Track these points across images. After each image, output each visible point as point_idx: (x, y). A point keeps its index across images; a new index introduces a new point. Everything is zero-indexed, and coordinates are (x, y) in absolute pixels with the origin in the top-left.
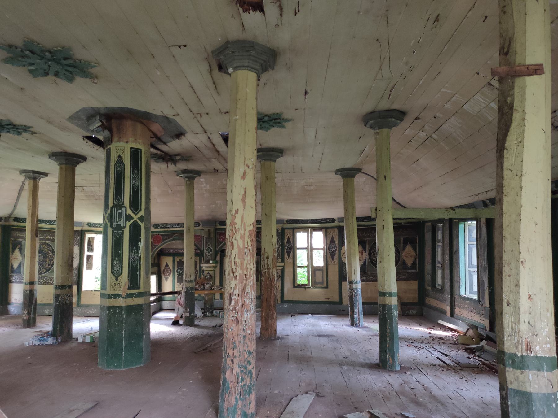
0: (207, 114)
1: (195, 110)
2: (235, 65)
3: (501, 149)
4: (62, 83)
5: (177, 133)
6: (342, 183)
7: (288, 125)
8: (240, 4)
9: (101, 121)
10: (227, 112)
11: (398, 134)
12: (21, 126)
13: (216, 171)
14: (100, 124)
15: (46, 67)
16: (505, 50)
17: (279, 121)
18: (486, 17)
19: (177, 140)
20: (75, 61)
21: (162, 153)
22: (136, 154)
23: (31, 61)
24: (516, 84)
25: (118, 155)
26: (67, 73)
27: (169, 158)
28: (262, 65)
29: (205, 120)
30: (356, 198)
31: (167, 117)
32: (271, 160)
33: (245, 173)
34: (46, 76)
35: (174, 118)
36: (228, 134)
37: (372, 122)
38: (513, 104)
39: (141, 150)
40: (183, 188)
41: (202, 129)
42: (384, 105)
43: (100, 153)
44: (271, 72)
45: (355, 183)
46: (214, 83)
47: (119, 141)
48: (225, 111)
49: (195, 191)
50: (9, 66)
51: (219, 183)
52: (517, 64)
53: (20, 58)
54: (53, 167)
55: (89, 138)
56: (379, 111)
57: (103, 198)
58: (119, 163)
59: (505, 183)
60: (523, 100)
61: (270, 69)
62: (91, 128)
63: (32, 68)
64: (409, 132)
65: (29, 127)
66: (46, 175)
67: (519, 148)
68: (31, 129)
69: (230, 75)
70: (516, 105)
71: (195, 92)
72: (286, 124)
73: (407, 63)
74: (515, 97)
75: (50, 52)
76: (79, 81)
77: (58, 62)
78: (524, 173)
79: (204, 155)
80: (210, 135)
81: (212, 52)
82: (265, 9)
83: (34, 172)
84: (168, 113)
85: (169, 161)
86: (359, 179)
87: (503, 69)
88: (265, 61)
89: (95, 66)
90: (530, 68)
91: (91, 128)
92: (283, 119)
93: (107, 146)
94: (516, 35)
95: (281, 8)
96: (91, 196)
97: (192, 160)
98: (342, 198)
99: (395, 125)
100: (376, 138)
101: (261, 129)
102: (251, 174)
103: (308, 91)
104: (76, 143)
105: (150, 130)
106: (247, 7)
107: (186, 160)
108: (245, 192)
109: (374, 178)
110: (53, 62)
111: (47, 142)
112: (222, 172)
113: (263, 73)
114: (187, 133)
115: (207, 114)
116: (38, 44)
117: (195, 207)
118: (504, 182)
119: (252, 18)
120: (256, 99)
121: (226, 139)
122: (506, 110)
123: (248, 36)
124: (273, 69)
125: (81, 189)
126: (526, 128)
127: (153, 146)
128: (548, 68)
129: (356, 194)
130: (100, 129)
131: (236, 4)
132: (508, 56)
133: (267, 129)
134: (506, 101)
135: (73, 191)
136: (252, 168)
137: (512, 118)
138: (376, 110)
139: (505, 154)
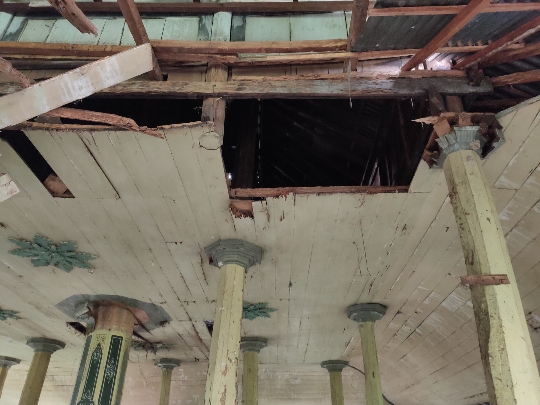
0: (194, 302)
1: (183, 298)
2: (225, 260)
3: (485, 356)
4: (61, 272)
5: (162, 320)
6: (328, 378)
7: (273, 314)
8: (233, 211)
9: (88, 308)
10: (214, 301)
11: (382, 327)
12: (9, 311)
13: (197, 360)
14: (88, 310)
15: (49, 258)
16: (470, 261)
17: (263, 310)
18: (448, 228)
19: (161, 328)
20: (77, 254)
21: (143, 340)
22: (116, 342)
23: (35, 252)
24: (487, 293)
25: (98, 342)
26: (67, 263)
27: (149, 346)
28: (250, 260)
29: (191, 308)
30: (345, 396)
31: (154, 305)
32: (254, 350)
33: (226, 368)
34: (46, 265)
35: (161, 305)
36: (213, 322)
37: (355, 314)
38: (488, 310)
39: (122, 338)
40: (160, 379)
41: (187, 317)
42: (365, 298)
43: (80, 339)
44: (258, 266)
45: (343, 378)
46: (204, 274)
47: (102, 328)
48: (212, 299)
49: (172, 383)
50: (15, 257)
51: (198, 373)
52: (483, 274)
53: (27, 250)
54: (27, 354)
55: (73, 324)
56: (361, 304)
57: (72, 389)
58: (97, 352)
59: (497, 393)
60: (496, 308)
61: (257, 264)
62: (78, 315)
63: (35, 258)
64: (393, 325)
65: (16, 312)
66: (17, 361)
67: (503, 355)
68: (17, 315)
69: (220, 268)
70: (491, 311)
71: (185, 282)
72: (270, 314)
73: (383, 263)
74: (488, 303)
75: (56, 246)
76: (77, 270)
77: (61, 254)
78: (514, 383)
79: (186, 344)
80: (194, 323)
81: (205, 248)
82: (254, 216)
83: (7, 358)
84: (156, 300)
85: (149, 349)
86: (347, 373)
87: (472, 278)
88: (252, 257)
89: (94, 258)
90: (496, 277)
91: (78, 315)
92: (268, 309)
93: (88, 334)
94: (476, 248)
95: (268, 216)
96: (60, 386)
97: (173, 348)
98: (330, 395)
99: (378, 318)
100: (360, 331)
101: (245, 318)
102: (232, 369)
103: (293, 283)
104: (58, 328)
105: (136, 318)
106: (239, 214)
107: (167, 348)
108: (225, 390)
109: (363, 373)
110: (56, 254)
111: (30, 327)
112: (203, 362)
113: (250, 266)
114: (172, 320)
115: (194, 302)
116: (48, 239)
117: (170, 401)
118: (496, 392)
119: (244, 222)
120: (243, 290)
121: (210, 327)
122: (482, 316)
123: (239, 236)
124: (260, 263)
125: (50, 378)
126: (505, 335)
127: (135, 333)
128: (512, 277)
129: (344, 391)
130: (86, 315)
131: (230, 211)
132: (473, 266)
133: (252, 318)
134: (480, 307)
135: (43, 381)
136: (235, 362)
137: (489, 324)
138: (358, 303)
139: (490, 361)
